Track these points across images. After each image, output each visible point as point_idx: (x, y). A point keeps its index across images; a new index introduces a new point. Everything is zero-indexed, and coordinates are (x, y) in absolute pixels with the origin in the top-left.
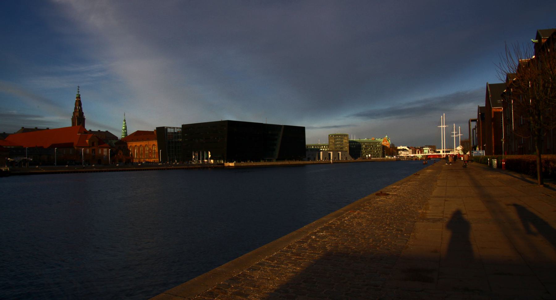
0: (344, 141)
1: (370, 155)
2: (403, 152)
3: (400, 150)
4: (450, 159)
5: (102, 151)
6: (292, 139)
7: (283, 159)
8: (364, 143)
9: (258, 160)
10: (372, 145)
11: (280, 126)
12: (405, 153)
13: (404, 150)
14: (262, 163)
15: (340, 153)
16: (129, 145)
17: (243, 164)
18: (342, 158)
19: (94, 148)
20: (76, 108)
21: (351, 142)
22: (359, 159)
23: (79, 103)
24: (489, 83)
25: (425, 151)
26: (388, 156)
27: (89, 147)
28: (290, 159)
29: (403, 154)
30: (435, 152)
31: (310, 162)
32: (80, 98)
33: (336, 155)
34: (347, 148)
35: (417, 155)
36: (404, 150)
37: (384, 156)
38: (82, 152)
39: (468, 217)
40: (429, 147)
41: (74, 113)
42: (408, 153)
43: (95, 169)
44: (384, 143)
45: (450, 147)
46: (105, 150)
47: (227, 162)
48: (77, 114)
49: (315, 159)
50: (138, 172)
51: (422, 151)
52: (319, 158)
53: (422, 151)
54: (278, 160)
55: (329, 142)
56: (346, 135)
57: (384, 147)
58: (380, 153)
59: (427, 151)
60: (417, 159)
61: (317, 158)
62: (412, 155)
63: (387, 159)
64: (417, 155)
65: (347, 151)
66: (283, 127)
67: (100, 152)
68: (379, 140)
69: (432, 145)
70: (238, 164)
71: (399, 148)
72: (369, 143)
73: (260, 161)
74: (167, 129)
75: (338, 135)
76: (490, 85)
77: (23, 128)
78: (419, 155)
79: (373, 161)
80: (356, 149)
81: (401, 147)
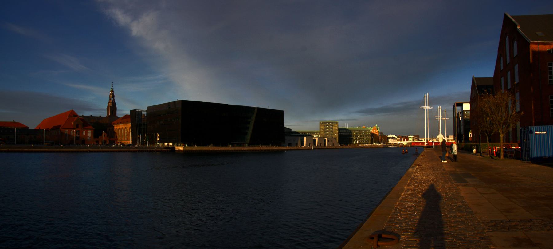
0: (334, 128)
1: (358, 142)
2: (392, 140)
3: (390, 138)
4: (124, 132)
5: (86, 133)
6: (269, 124)
7: (258, 144)
8: (355, 131)
9: (206, 145)
10: (362, 133)
11: (254, 108)
12: (394, 140)
13: (393, 138)
14: (230, 148)
15: (326, 139)
16: (115, 128)
17: (196, 148)
18: (328, 144)
19: (77, 130)
20: (110, 100)
21: (339, 130)
22: (349, 146)
23: (113, 95)
24: (475, 77)
25: (410, 139)
26: (376, 142)
27: (74, 129)
28: (267, 144)
29: (391, 141)
30: (418, 140)
31: (287, 148)
32: (113, 91)
33: (322, 139)
34: (336, 135)
35: (403, 142)
36: (393, 138)
37: (372, 143)
38: (82, 135)
39: (439, 188)
40: (414, 136)
41: (108, 104)
42: (395, 140)
43: (100, 149)
44: (374, 132)
45: (434, 134)
46: (89, 132)
47: (177, 145)
48: (110, 104)
49: (297, 145)
50: (49, 154)
51: (407, 140)
52: (302, 144)
53: (407, 140)
54: (250, 145)
55: (320, 129)
56: (337, 123)
57: (373, 135)
58: (369, 140)
59: (411, 139)
60: (402, 146)
61: (299, 142)
62: (399, 142)
63: (375, 146)
64: (403, 142)
65: (335, 139)
66: (256, 110)
67: (84, 134)
68: (370, 128)
69: (416, 134)
70: (190, 148)
71: (389, 136)
72: (360, 131)
73: (227, 146)
74: (141, 112)
75: (329, 122)
76: (476, 78)
77: (73, 114)
78: (405, 143)
79: (361, 147)
80: (345, 136)
81: (391, 136)
